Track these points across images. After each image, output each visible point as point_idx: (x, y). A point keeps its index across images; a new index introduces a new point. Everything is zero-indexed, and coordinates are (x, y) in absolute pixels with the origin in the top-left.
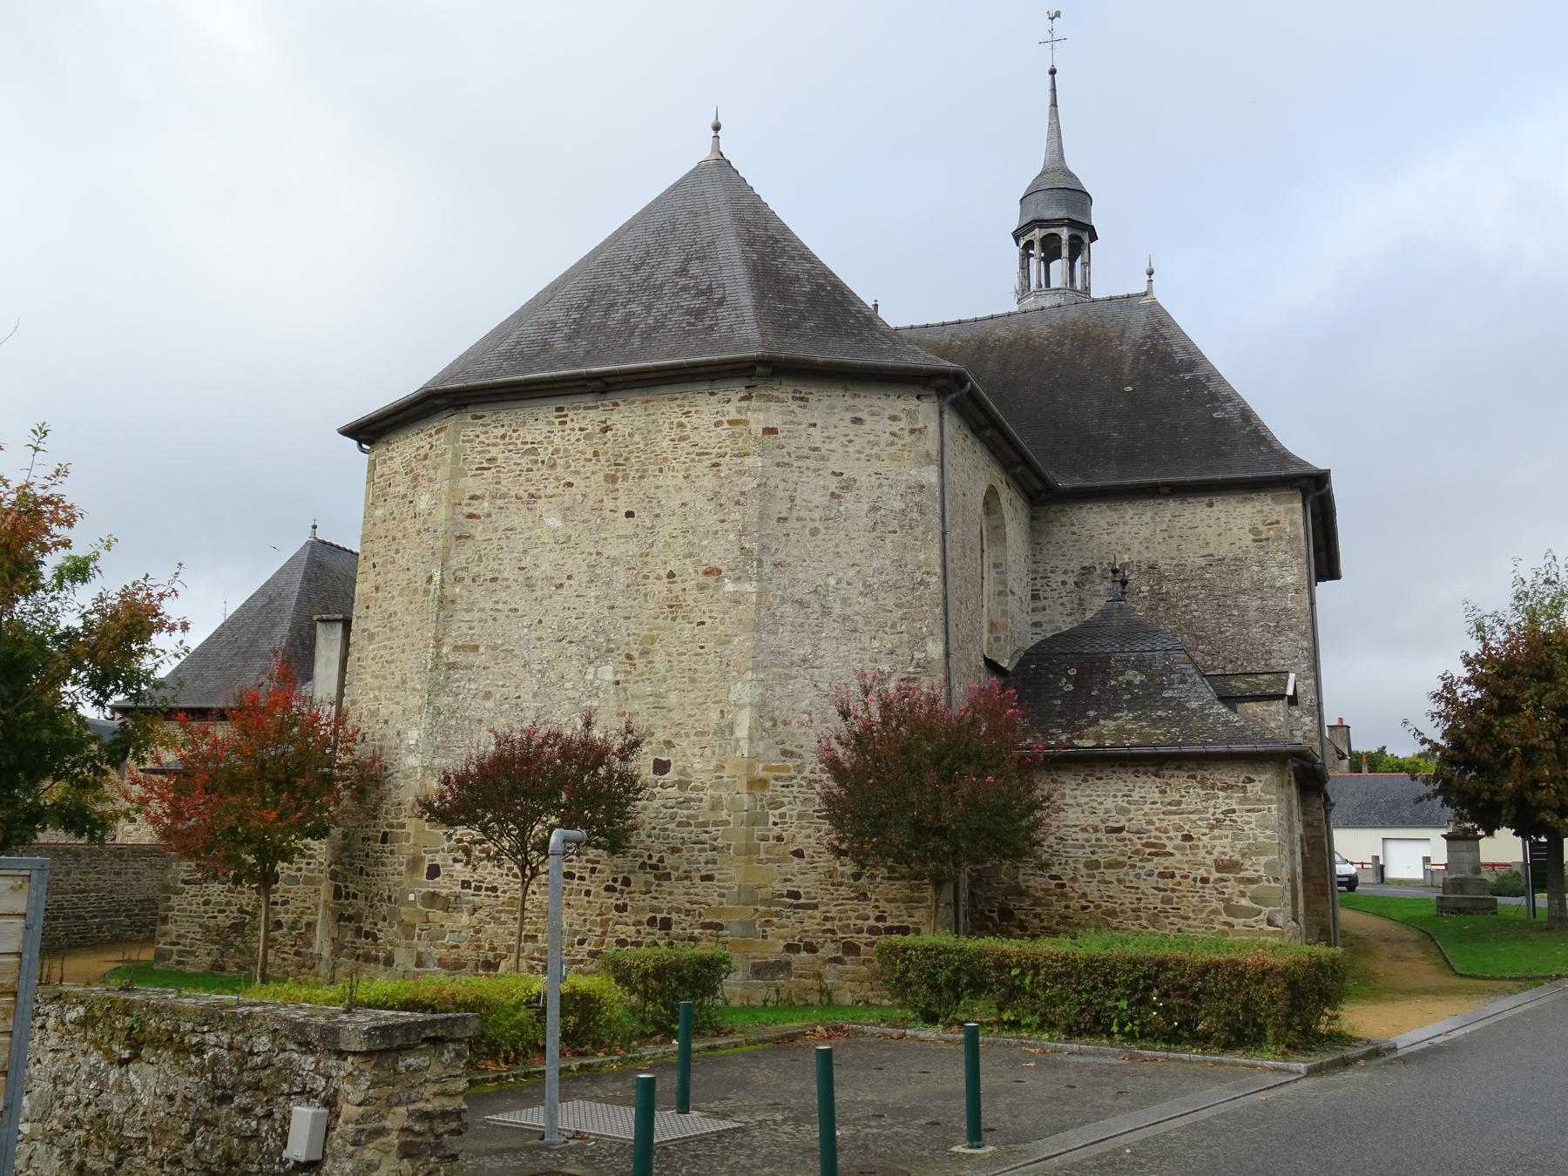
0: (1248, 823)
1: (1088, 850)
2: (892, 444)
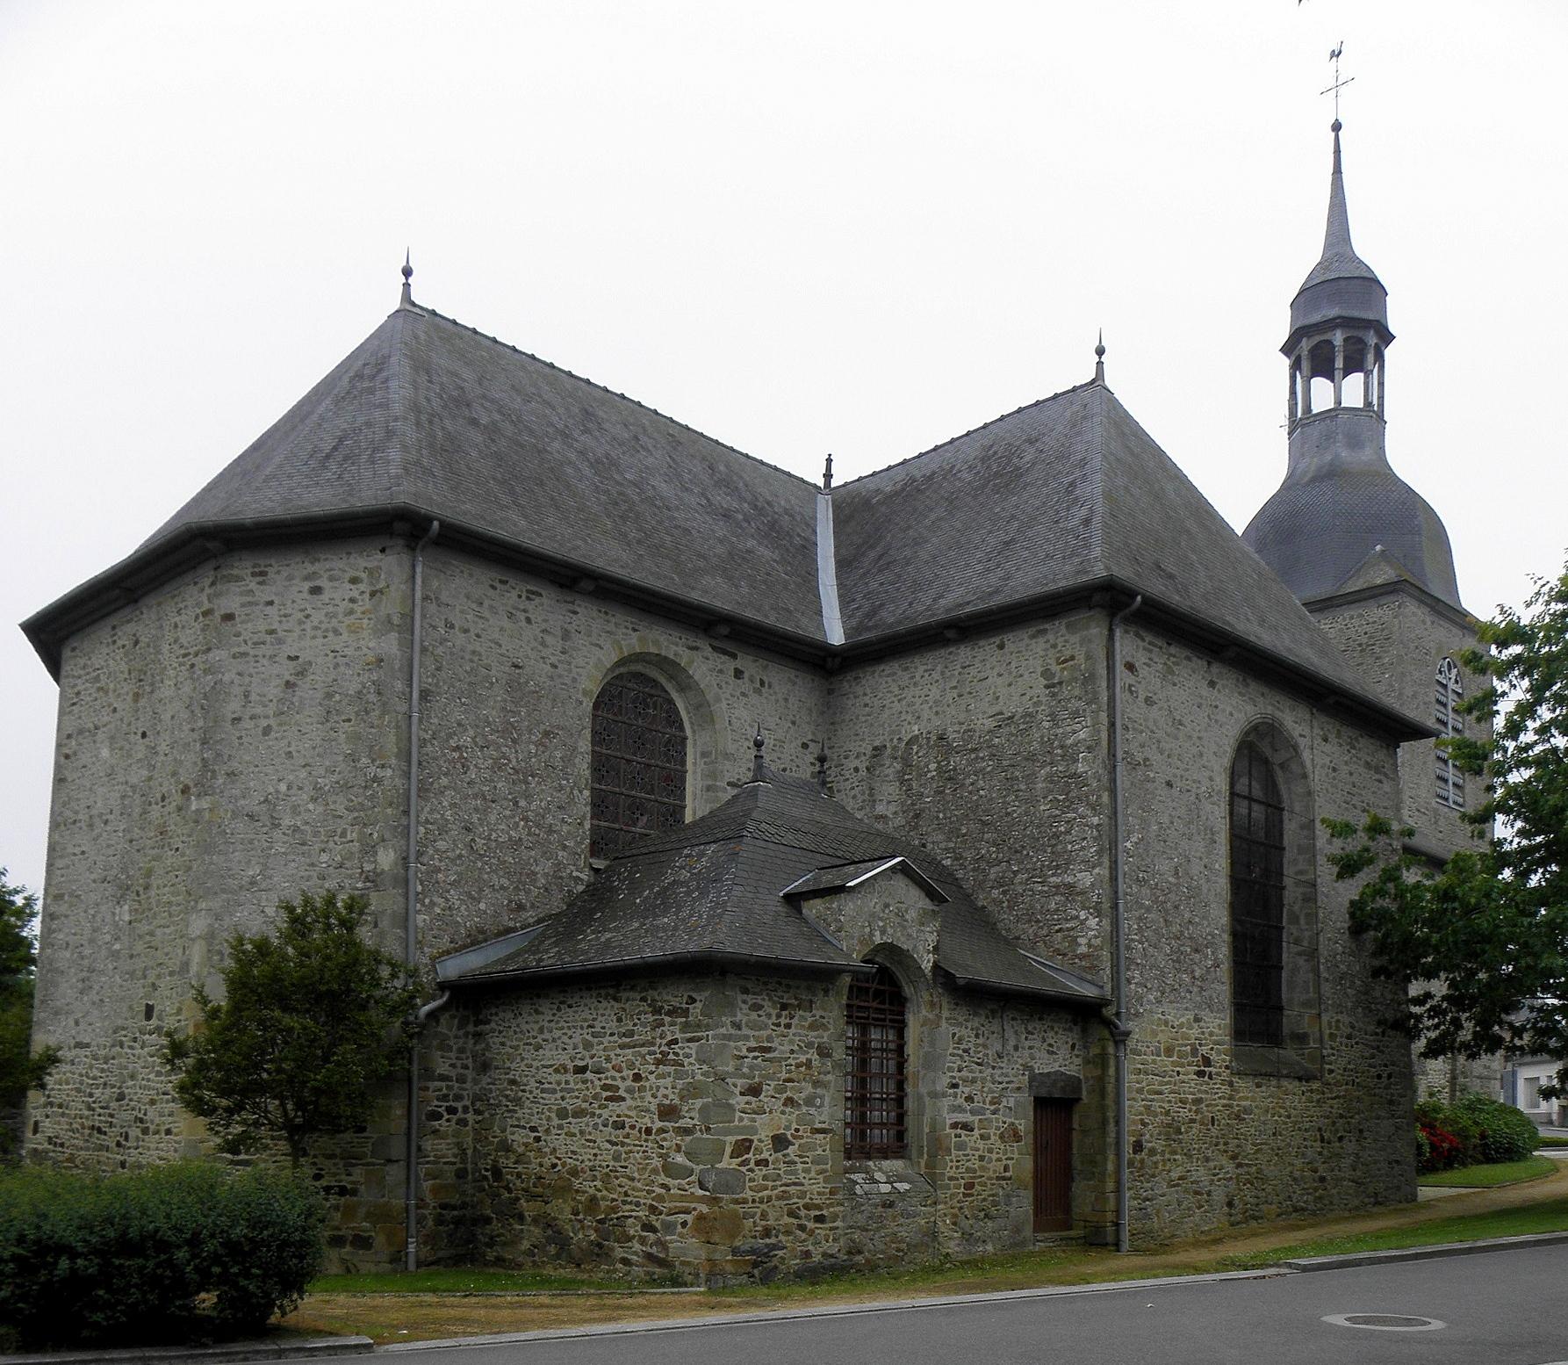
0: (688, 1056)
1: (559, 1095)
2: (351, 612)
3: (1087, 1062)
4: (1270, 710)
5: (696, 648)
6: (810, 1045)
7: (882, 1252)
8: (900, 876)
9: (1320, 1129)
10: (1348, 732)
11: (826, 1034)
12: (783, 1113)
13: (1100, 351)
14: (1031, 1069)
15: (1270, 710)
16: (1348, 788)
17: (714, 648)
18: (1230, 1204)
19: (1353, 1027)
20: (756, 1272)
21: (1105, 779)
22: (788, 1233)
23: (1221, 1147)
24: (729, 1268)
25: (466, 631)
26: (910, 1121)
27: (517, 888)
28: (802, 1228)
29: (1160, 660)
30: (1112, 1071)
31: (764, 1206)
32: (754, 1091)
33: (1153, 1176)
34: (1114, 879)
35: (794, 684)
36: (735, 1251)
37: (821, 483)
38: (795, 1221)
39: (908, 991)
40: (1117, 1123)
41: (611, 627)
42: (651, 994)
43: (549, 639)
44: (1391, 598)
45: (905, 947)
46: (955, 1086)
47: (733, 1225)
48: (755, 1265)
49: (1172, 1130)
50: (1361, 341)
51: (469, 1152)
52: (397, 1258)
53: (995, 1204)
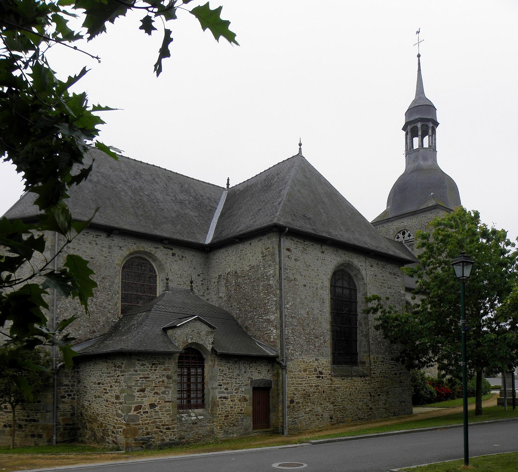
0: (122, 380)
3: (273, 375)
4: (347, 259)
5: (158, 248)
6: (164, 375)
7: (192, 438)
8: (198, 321)
9: (370, 392)
10: (381, 263)
11: (170, 372)
12: (154, 397)
13: (300, 145)
14: (251, 378)
15: (347, 259)
16: (382, 281)
17: (164, 247)
18: (331, 418)
19: (384, 358)
20: (144, 446)
21: (278, 287)
22: (156, 433)
23: (327, 400)
24: (133, 445)
25: (74, 249)
26: (206, 396)
27: (93, 326)
28: (161, 432)
29: (300, 247)
30: (281, 378)
31: (147, 426)
32: (143, 390)
33: (299, 410)
34: (281, 317)
35: (194, 256)
36: (135, 440)
37: (225, 187)
38: (159, 430)
39: (204, 356)
40: (283, 395)
41: (127, 244)
42: (114, 361)
43: (104, 249)
44: (434, 210)
45: (201, 343)
46: (221, 385)
47: (135, 432)
48: (143, 444)
49: (306, 396)
50: (427, 126)
51: (76, 408)
52: (50, 441)
53: (237, 422)
